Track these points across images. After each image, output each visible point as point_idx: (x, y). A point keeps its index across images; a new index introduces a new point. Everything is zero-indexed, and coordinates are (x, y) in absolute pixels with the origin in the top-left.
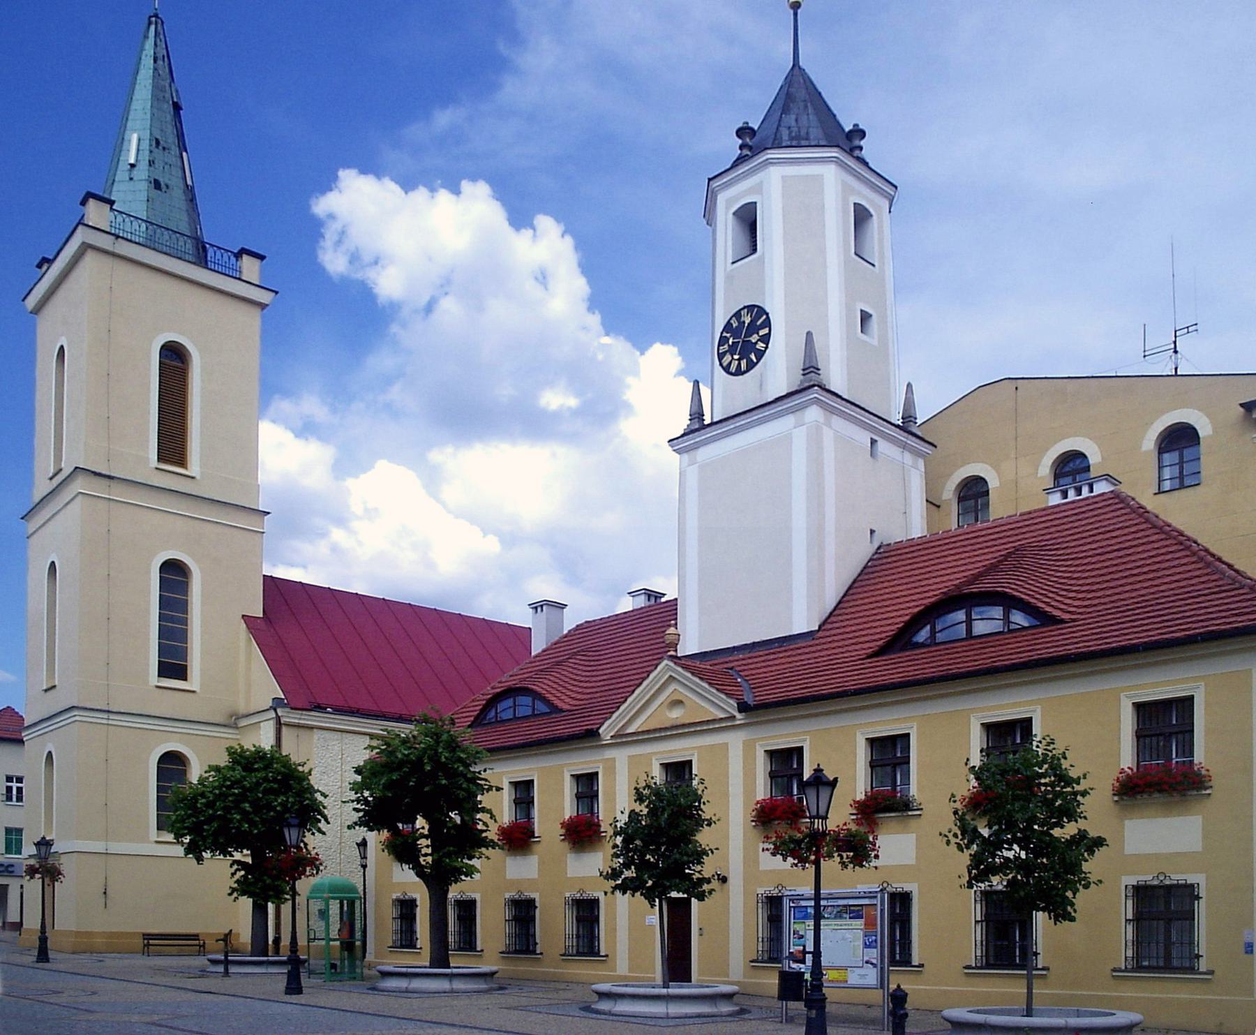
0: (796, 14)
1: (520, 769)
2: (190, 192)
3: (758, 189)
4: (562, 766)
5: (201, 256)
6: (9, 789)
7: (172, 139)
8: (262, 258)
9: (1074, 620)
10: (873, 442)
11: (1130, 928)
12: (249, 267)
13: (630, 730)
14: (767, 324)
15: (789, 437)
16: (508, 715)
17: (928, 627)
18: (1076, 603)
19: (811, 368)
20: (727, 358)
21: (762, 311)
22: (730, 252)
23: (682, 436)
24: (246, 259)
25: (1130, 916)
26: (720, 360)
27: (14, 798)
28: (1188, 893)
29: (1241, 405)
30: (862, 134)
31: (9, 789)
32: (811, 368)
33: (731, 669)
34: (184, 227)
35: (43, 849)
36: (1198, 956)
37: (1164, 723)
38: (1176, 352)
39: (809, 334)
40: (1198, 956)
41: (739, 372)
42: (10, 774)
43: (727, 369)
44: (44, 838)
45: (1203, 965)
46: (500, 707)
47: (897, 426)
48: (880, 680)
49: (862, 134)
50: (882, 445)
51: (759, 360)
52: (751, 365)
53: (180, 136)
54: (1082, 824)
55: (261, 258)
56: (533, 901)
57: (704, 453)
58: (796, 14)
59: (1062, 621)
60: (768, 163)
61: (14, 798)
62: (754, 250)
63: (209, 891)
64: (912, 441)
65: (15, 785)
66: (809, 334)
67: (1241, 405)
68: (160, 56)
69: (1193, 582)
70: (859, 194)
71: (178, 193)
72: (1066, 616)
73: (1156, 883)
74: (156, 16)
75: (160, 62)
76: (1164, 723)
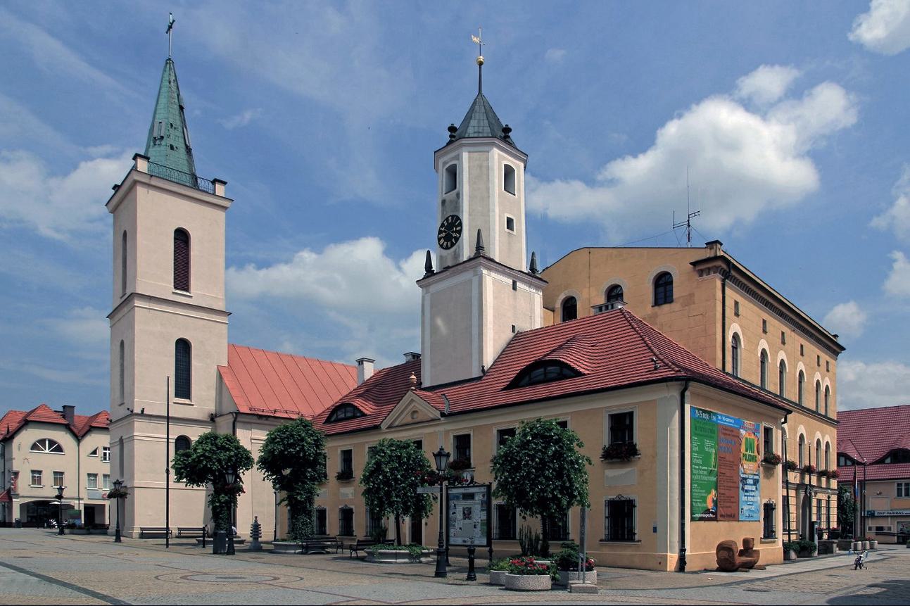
0: (480, 68)
1: (346, 444)
2: (188, 150)
3: (458, 157)
4: (364, 443)
5: (195, 184)
6: (105, 454)
7: (178, 123)
8: (225, 183)
9: (589, 374)
10: (514, 283)
11: (607, 520)
12: (220, 190)
13: (396, 423)
14: (461, 224)
15: (471, 281)
16: (343, 416)
17: (528, 377)
18: (592, 365)
19: (479, 247)
20: (442, 241)
21: (458, 218)
22: (444, 188)
23: (423, 279)
24: (218, 186)
25: (607, 515)
26: (439, 241)
27: (108, 459)
28: (630, 504)
29: (691, 263)
30: (510, 130)
31: (105, 454)
32: (479, 247)
33: (444, 394)
34: (186, 169)
35: (117, 486)
36: (635, 534)
37: (622, 425)
38: (689, 226)
39: (479, 230)
40: (635, 534)
41: (447, 248)
42: (105, 446)
43: (441, 246)
44: (118, 480)
45: (637, 537)
46: (339, 413)
47: (526, 273)
48: (503, 402)
49: (510, 130)
50: (519, 284)
51: (456, 242)
52: (453, 245)
53: (183, 121)
54: (255, 467)
55: (225, 183)
56: (352, 509)
57: (433, 289)
58: (480, 68)
59: (584, 375)
60: (462, 145)
61: (108, 459)
62: (455, 188)
63: (191, 506)
64: (534, 280)
65: (108, 452)
66: (479, 230)
67: (691, 263)
68: (172, 80)
69: (631, 355)
70: (509, 160)
71: (182, 150)
72: (586, 372)
73: (618, 499)
74: (169, 59)
75: (172, 84)
76: (622, 425)
